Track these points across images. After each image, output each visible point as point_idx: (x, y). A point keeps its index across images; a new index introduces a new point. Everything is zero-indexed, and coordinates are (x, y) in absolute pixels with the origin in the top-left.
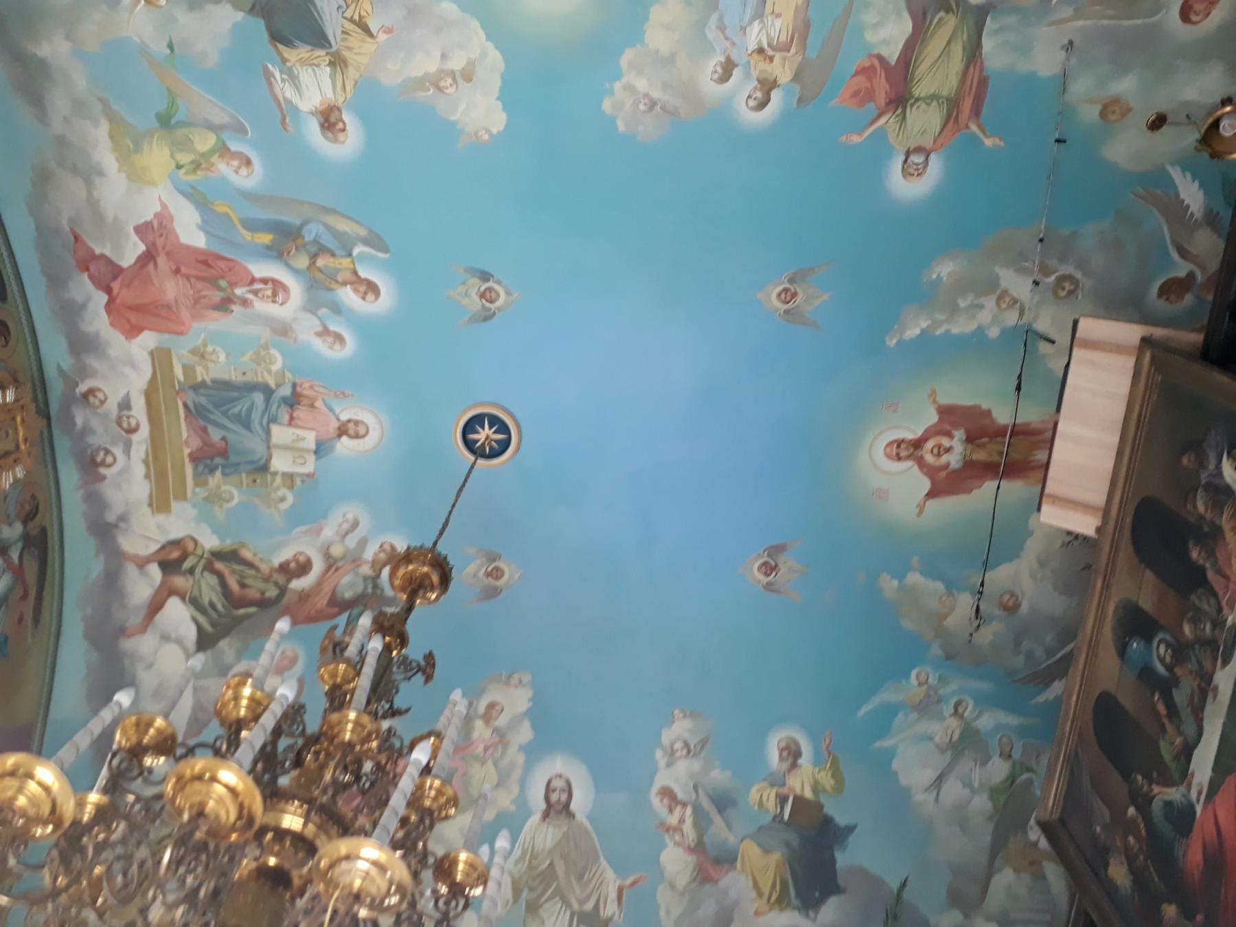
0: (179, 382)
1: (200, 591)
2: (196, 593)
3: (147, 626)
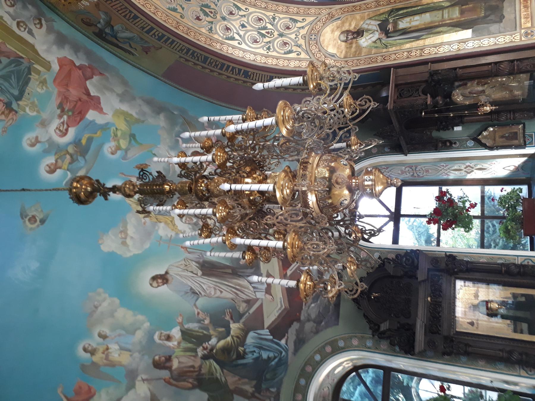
0: (34, 64)
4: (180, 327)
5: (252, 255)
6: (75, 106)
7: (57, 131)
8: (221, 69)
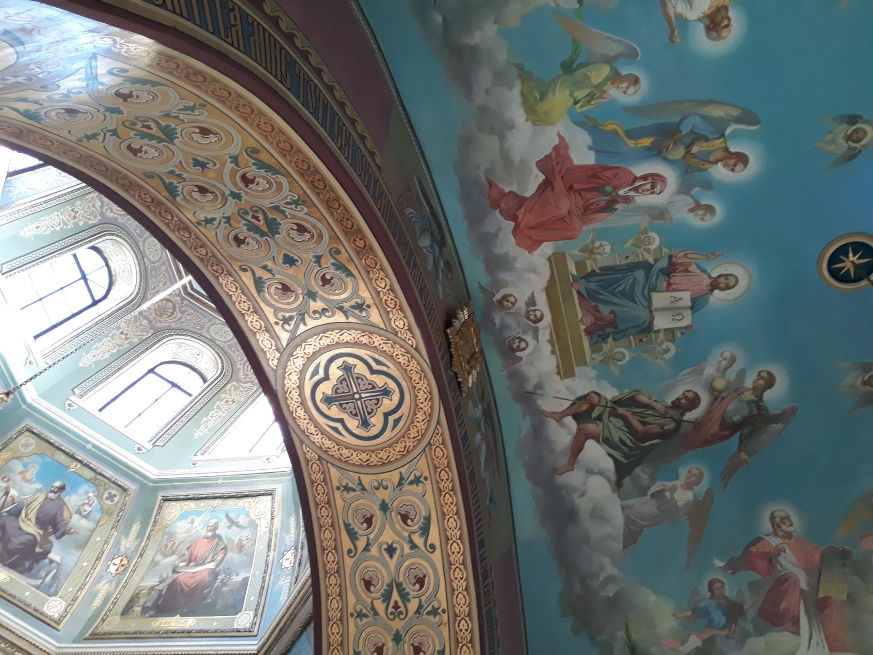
0: (573, 275)
1: (610, 431)
2: (607, 434)
3: (574, 463)
7: (657, 189)
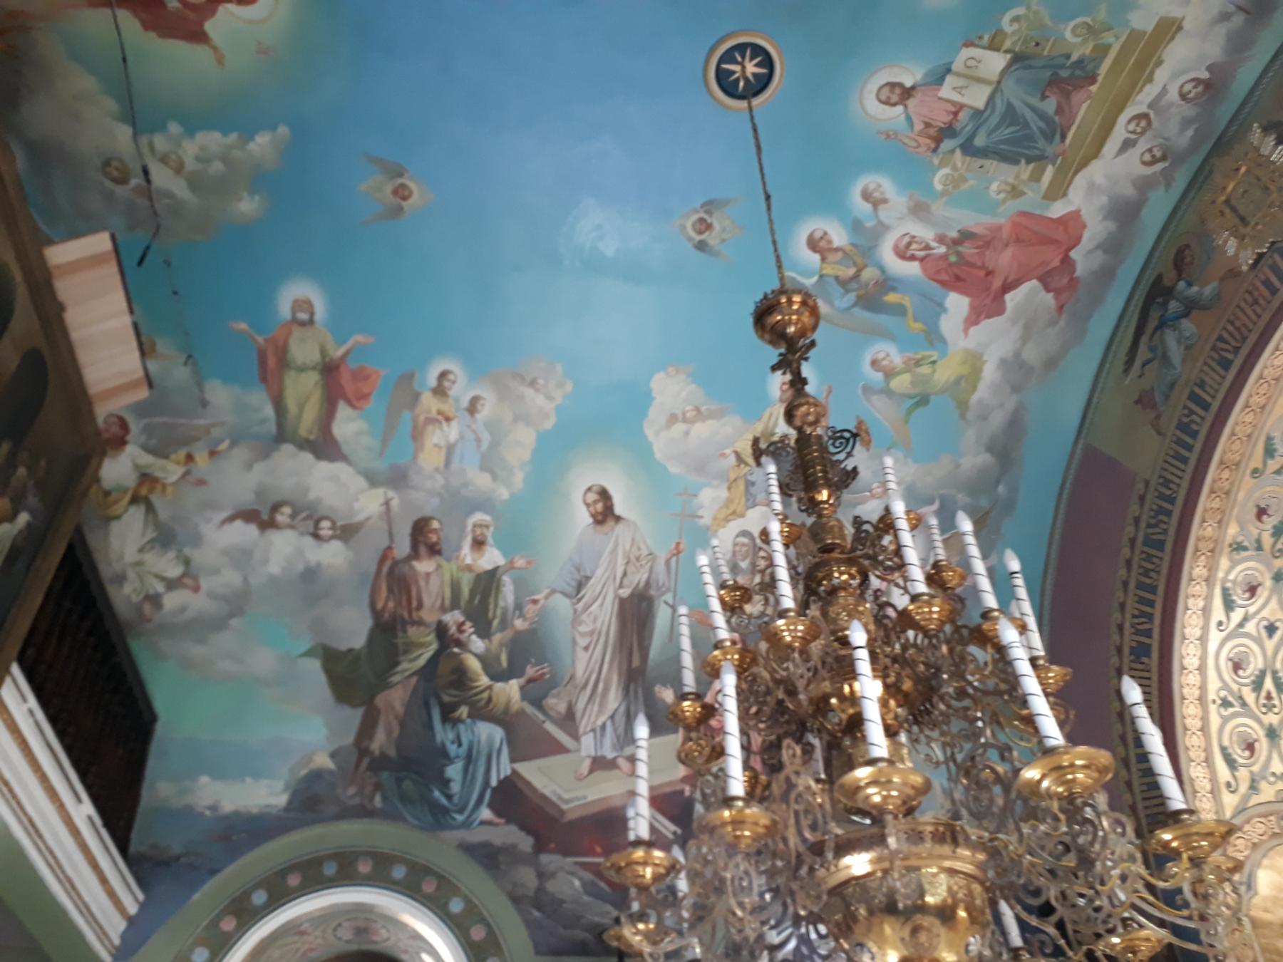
4: (505, 565)
5: (695, 717)
6: (972, 265)
7: (907, 239)
8: (1140, 586)
